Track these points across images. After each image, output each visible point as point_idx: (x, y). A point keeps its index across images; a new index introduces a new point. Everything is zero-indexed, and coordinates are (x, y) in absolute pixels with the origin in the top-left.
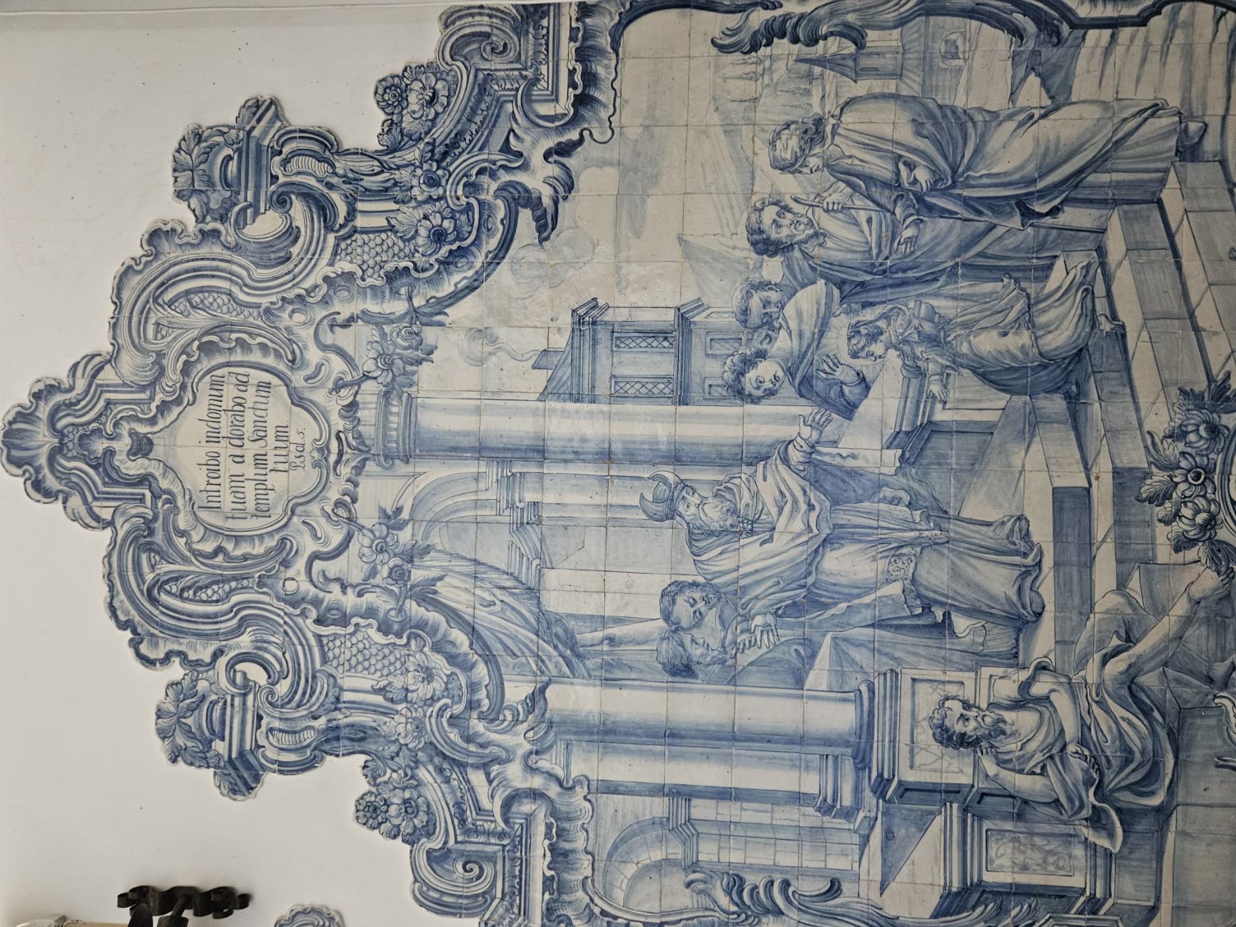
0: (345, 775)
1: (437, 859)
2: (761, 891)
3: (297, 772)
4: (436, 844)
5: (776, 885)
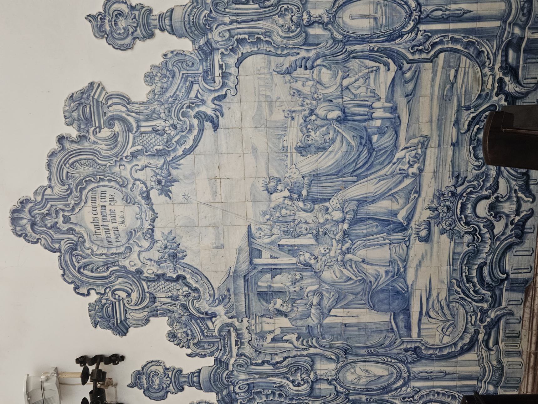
3: (142, 326)
4: (196, 341)
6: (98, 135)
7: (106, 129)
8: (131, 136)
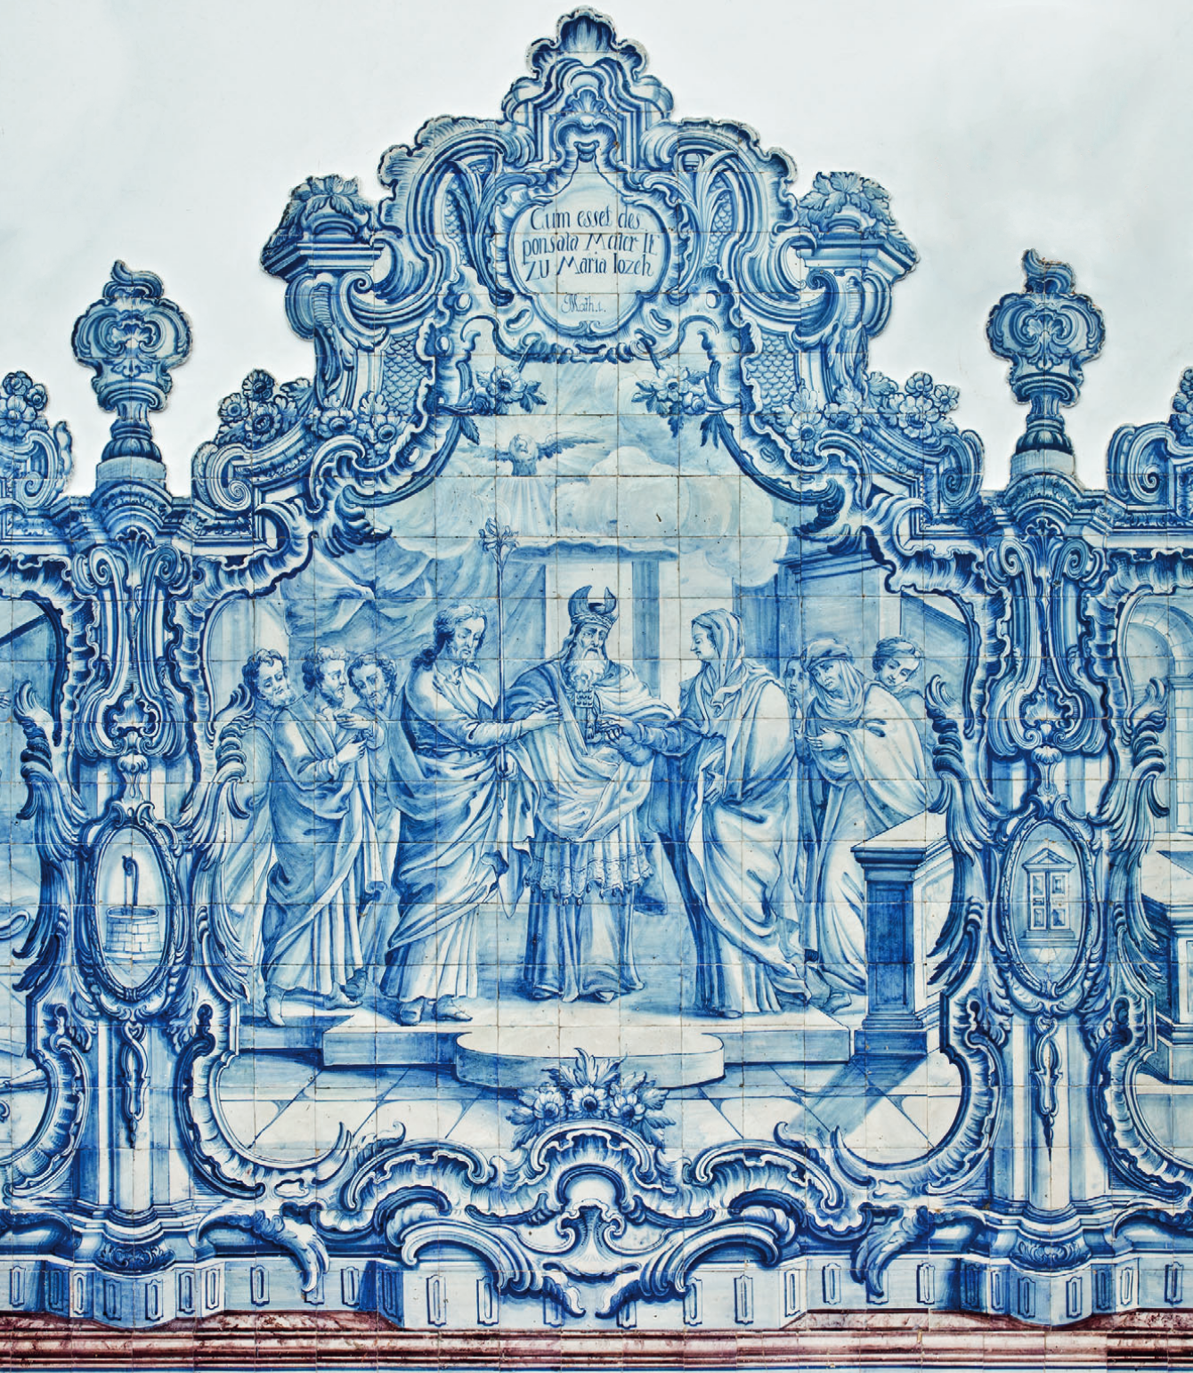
0: (295, 362)
1: (1158, 449)
2: (1153, 747)
4: (1172, 446)
5: (1159, 761)
6: (791, 251)
7: (806, 272)
8: (790, 329)
